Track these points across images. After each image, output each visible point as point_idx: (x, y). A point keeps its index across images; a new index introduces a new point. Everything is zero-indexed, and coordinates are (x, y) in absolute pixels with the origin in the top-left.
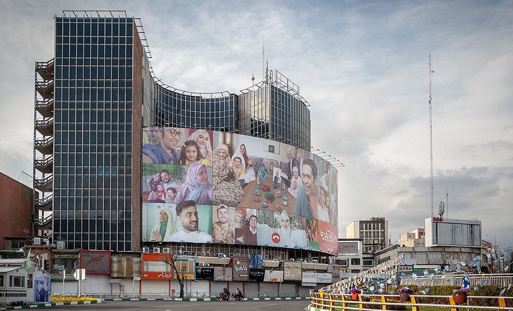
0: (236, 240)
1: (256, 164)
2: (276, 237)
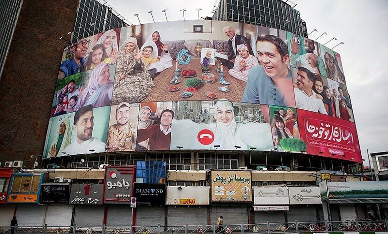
0: (137, 145)
1: (175, 48)
2: (206, 136)
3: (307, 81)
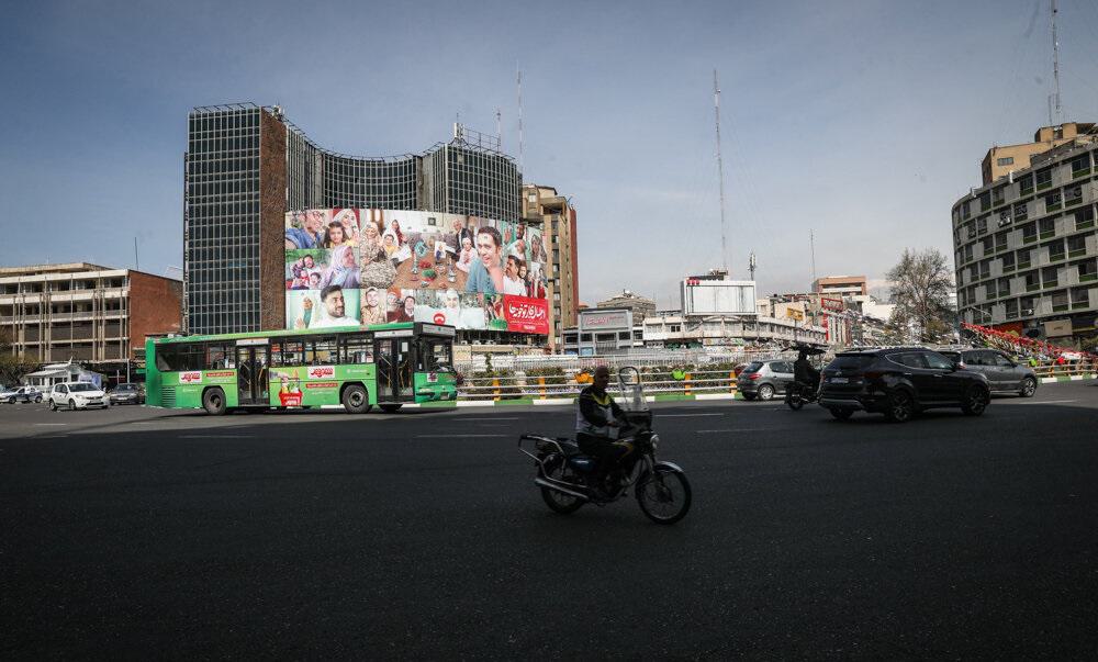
3: (514, 269)
